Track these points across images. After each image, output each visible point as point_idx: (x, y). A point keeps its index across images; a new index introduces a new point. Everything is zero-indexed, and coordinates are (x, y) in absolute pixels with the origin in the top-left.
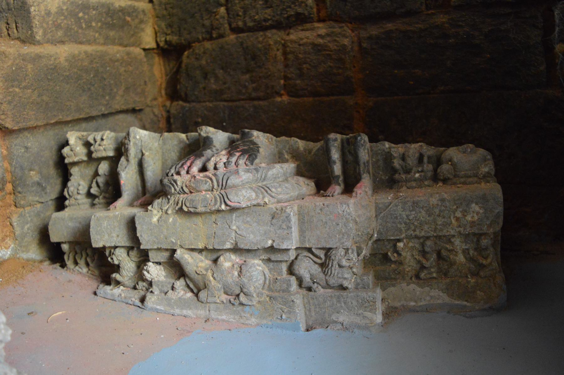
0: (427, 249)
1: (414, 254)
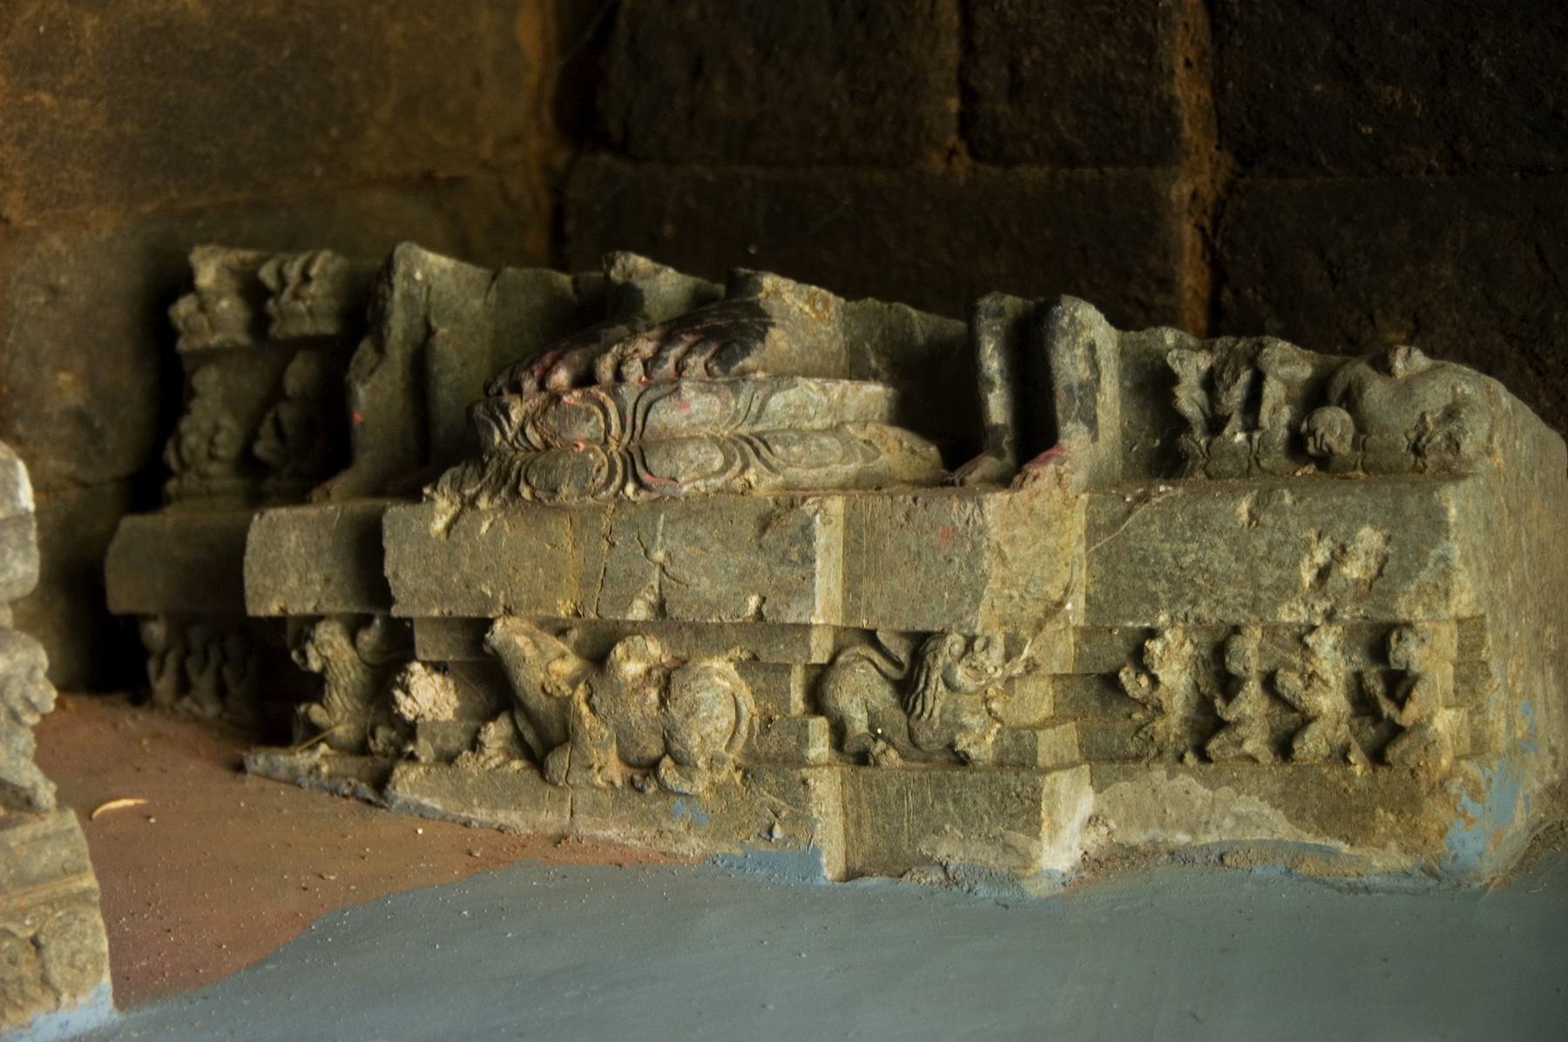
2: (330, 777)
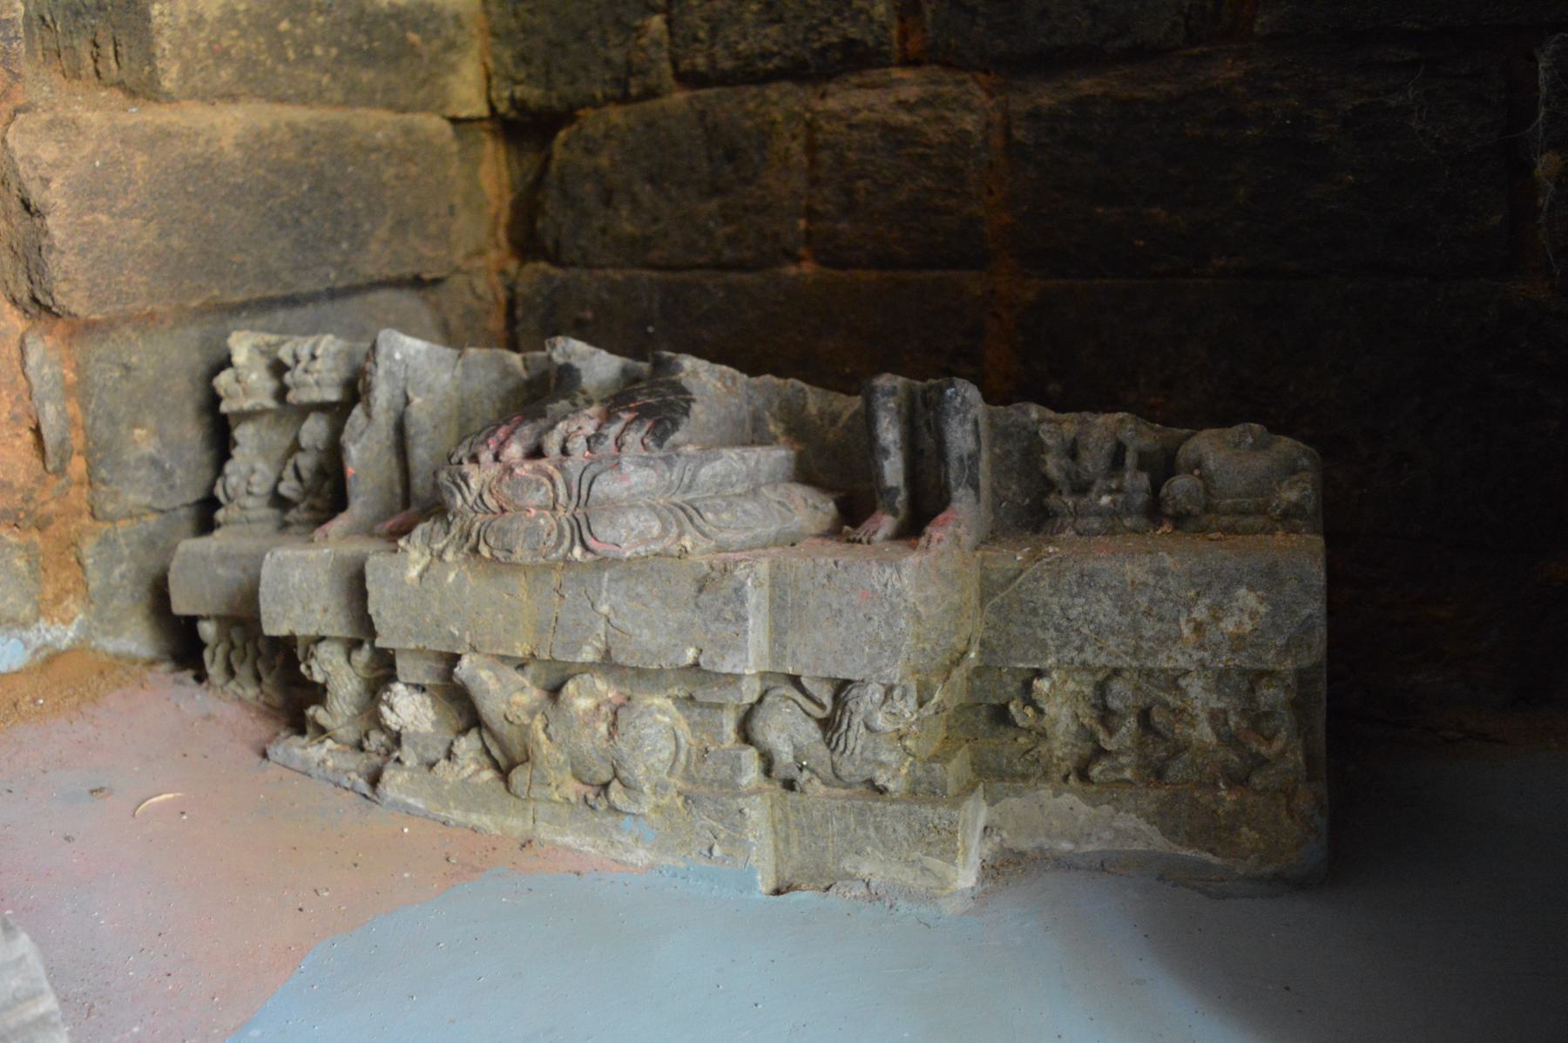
0: (1114, 703)
1: (1080, 712)
2: (335, 770)
